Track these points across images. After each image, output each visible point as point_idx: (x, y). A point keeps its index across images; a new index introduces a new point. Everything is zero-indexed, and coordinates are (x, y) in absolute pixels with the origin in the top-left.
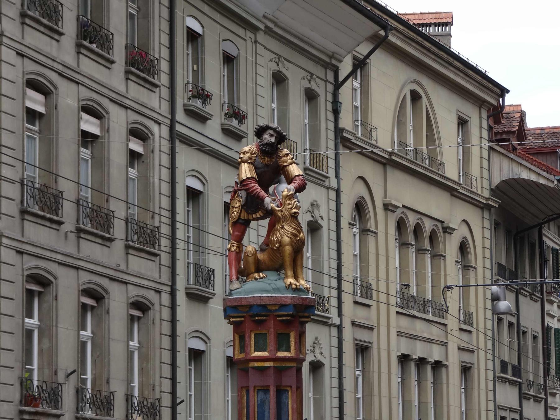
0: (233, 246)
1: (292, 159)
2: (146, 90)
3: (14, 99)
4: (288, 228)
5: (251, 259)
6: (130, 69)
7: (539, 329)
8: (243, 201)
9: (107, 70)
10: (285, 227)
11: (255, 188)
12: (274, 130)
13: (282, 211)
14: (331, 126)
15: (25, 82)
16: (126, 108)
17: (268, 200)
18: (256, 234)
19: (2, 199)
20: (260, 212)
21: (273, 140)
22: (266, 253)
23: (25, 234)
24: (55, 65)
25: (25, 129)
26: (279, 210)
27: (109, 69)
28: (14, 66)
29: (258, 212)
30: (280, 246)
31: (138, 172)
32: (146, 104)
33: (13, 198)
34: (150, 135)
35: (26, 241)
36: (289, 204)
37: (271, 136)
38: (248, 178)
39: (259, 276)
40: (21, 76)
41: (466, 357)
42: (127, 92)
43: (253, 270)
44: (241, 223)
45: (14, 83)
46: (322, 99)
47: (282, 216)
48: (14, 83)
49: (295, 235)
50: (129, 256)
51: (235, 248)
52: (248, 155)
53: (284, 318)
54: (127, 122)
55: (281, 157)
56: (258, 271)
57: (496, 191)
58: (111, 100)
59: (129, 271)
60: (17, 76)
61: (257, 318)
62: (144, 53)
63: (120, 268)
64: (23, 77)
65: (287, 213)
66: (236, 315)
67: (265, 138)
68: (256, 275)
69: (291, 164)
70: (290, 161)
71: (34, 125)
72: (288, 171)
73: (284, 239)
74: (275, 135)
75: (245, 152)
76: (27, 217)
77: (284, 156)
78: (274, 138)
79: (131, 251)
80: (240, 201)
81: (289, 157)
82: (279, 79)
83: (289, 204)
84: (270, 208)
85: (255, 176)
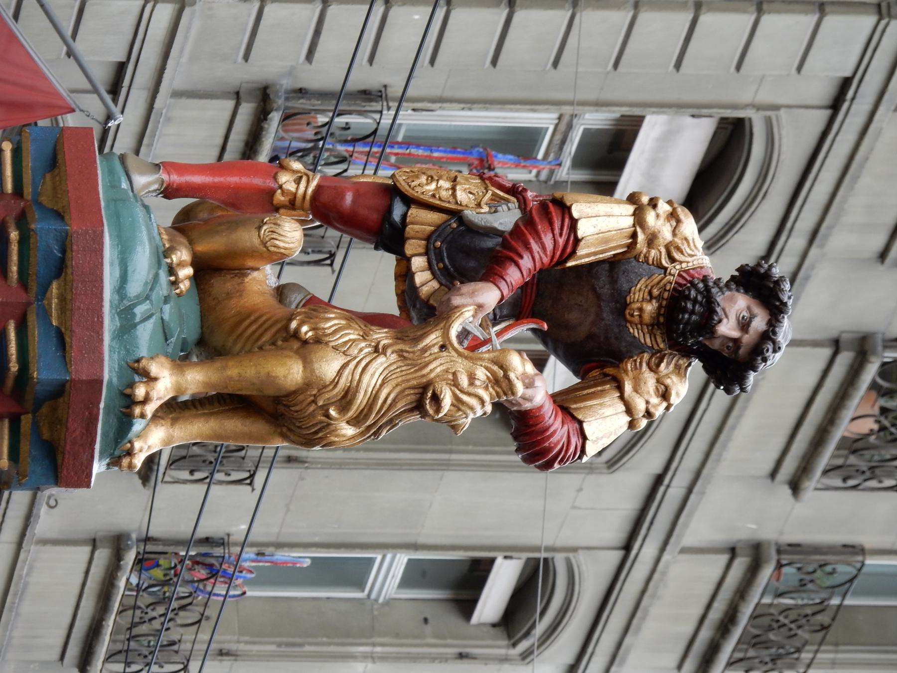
0: (298, 181)
1: (648, 414)
2: (688, 628)
3: (678, 66)
5: (248, 237)
6: (767, 561)
8: (480, 217)
9: (769, 466)
10: (382, 359)
11: (535, 247)
12: (768, 336)
13: (443, 347)
15: (740, 114)
16: (627, 547)
17: (490, 296)
19: (318, 7)
21: (727, 328)
22: (272, 301)
23: (184, 101)
24: (795, 243)
25: (567, 110)
27: (773, 475)
28: (799, 69)
29: (435, 276)
30: (305, 342)
31: (389, 602)
32: (639, 629)
33: (317, 55)
34: (524, 645)
35: (157, 105)
36: (472, 378)
37: (744, 325)
38: (574, 223)
39: (181, 264)
40: (764, 97)
42: (683, 551)
43: (201, 248)
44: (389, 210)
45: (738, 67)
47: (424, 350)
48: (738, 67)
49: (345, 400)
50: (87, 549)
51: (291, 187)
52: (666, 233)
53: (13, 349)
54: (575, 550)
55: (654, 369)
56: (205, 270)
58: (659, 480)
59: (31, 550)
60: (762, 78)
61: (14, 235)
62: (824, 618)
63: (44, 509)
64: (759, 108)
65: (436, 368)
66: (29, 163)
67: (732, 300)
69: (629, 411)
70: (640, 406)
71: (578, 162)
72: (602, 394)
73: (331, 354)
74: (748, 339)
75: (678, 221)
76: (247, 110)
77: (658, 381)
78: (735, 334)
79: (103, 555)
80: (479, 205)
81: (655, 400)
83: (472, 378)
84: (456, 301)
85: (585, 255)
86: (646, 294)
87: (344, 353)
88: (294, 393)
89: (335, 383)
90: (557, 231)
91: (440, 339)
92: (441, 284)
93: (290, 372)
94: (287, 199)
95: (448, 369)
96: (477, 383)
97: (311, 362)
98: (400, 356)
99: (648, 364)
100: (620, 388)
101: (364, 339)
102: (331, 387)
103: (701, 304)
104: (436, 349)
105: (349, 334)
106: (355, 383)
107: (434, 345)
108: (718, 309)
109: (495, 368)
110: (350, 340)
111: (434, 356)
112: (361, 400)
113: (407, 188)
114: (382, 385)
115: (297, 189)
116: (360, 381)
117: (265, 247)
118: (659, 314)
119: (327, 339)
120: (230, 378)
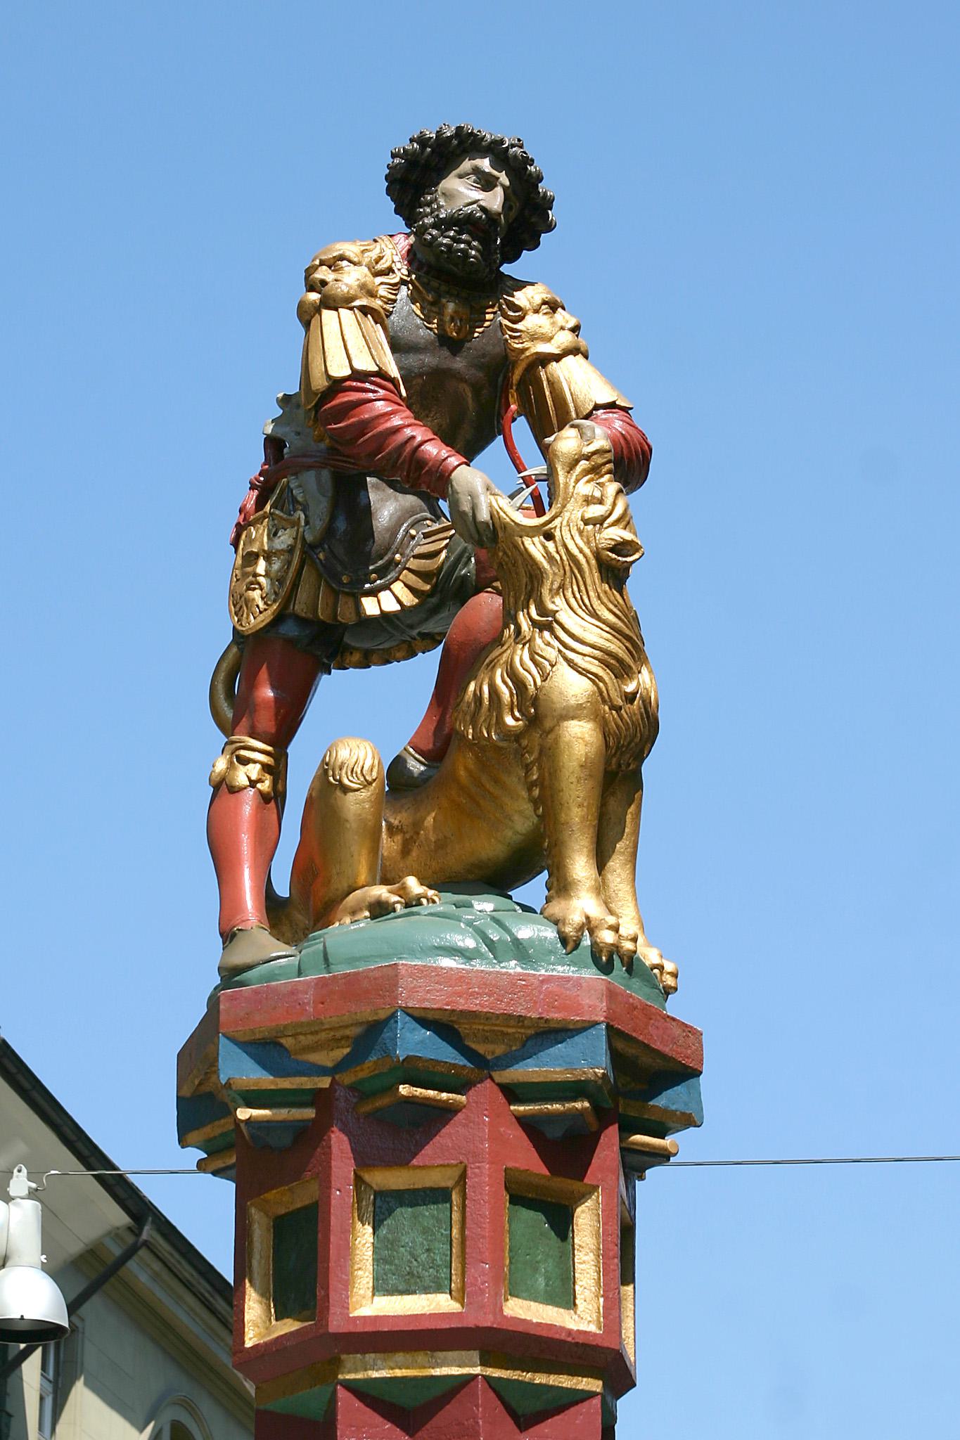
13: (549, 536)
20: (398, 587)
21: (494, 200)
26: (532, 532)
29: (387, 587)
36: (589, 501)
37: (487, 183)
38: (357, 375)
39: (402, 891)
44: (290, 642)
47: (550, 558)
65: (576, 544)
68: (381, 892)
74: (504, 179)
75: (342, 258)
77: (536, 311)
78: (499, 191)
83: (589, 501)
86: (434, 309)
87: (552, 666)
88: (605, 735)
89: (595, 678)
90: (371, 395)
91: (536, 539)
92: (397, 579)
93: (580, 737)
94: (268, 776)
95: (579, 529)
96: (597, 494)
97: (566, 708)
98: (557, 593)
99: (514, 322)
100: (545, 360)
101: (529, 641)
102: (601, 685)
103: (459, 233)
104: (550, 545)
105: (521, 660)
106: (597, 653)
107: (545, 547)
108: (468, 210)
109: (579, 469)
110: (532, 659)
111: (560, 548)
112: (615, 647)
113: (269, 612)
114: (598, 618)
115: (255, 762)
116: (593, 647)
117: (370, 783)
118: (457, 296)
119: (531, 688)
120: (584, 819)
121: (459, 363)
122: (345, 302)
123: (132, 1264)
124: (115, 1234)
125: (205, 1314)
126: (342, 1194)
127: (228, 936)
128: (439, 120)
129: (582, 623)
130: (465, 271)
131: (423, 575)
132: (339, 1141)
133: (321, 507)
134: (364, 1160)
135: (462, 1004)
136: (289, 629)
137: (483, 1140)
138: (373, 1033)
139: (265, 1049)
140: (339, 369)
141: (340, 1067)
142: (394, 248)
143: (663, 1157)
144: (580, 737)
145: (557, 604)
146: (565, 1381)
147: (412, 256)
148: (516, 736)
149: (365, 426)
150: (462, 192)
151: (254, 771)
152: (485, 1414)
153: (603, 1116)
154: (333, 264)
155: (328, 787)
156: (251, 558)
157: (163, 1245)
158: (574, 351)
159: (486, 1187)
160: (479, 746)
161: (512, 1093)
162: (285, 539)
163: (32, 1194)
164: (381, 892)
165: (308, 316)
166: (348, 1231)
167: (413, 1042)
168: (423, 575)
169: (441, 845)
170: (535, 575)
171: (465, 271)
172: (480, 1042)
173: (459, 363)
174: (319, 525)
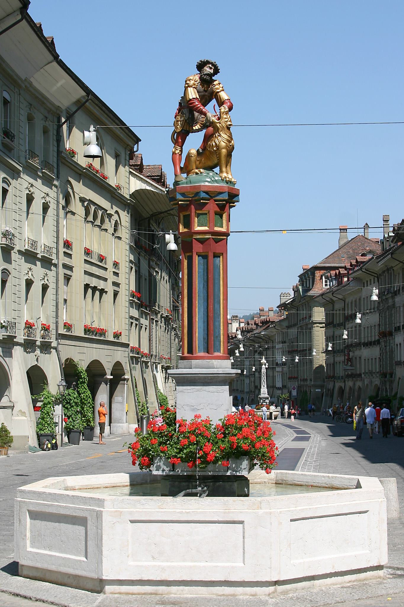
4: (224, 136)
7: (147, 274)
14: (56, 149)
18: (194, 142)
30: (218, 149)
36: (226, 118)
37: (211, 68)
39: (200, 171)
41: (68, 272)
44: (183, 133)
46: (51, 133)
57: (132, 195)
65: (224, 125)
67: (205, 70)
68: (197, 171)
82: (30, 119)
83: (226, 118)
93: (224, 151)
121: (206, 94)
122: (191, 86)
123: (87, 104)
124: (83, 97)
125: (101, 111)
126: (193, 214)
127: (176, 175)
128: (204, 58)
129: (224, 136)
130: (207, 81)
131: (202, 124)
132: (193, 207)
133: (187, 115)
134: (196, 209)
135: (209, 190)
136: (183, 131)
137: (212, 207)
138: (197, 194)
139: (183, 194)
140: (191, 98)
141: (193, 197)
142: (197, 78)
143: (234, 206)
144: (224, 151)
145: (221, 133)
146: (222, 237)
147: (200, 78)
148: (215, 151)
149: (195, 106)
150: (208, 70)
151: (178, 151)
152: (212, 242)
153: (227, 203)
154: (189, 80)
155: (189, 156)
156: (178, 121)
157: (94, 99)
158: (223, 90)
159: (212, 213)
160: (210, 151)
161: (215, 201)
162: (182, 119)
163: (94, 131)
164: (197, 171)
165: (186, 88)
166: (194, 219)
167: (203, 195)
168: (202, 124)
169: (205, 163)
170: (218, 129)
171: (207, 81)
172: (211, 194)
173: (206, 94)
174: (187, 117)
